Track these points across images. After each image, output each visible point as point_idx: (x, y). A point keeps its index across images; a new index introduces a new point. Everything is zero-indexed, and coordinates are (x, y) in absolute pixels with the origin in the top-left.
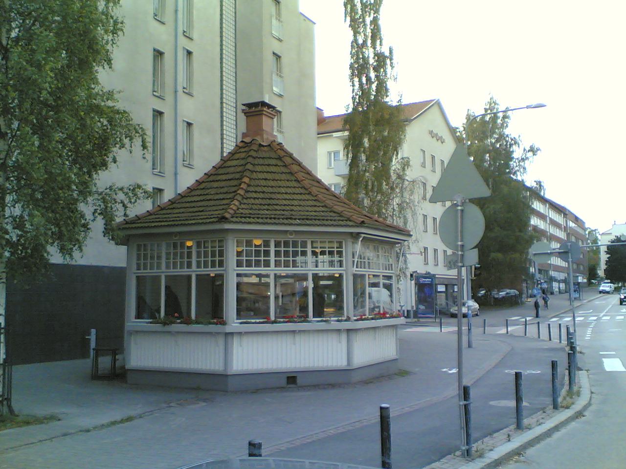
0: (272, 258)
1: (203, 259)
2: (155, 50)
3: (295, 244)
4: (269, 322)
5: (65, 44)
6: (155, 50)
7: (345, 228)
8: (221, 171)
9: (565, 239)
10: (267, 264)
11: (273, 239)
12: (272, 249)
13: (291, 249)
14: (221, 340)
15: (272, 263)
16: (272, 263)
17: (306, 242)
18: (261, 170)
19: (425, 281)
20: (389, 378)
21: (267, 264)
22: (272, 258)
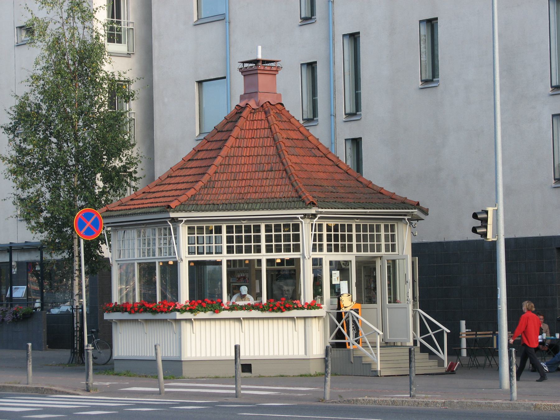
0: (263, 244)
1: (214, 245)
2: (197, 82)
3: (248, 229)
4: (71, 260)
5: (43, 178)
6: (197, 82)
7: (149, 216)
8: (169, 180)
9: (349, 163)
10: (258, 250)
11: (224, 225)
12: (263, 234)
13: (234, 235)
14: (300, 324)
15: (263, 249)
16: (263, 249)
17: (259, 226)
18: (290, 145)
19: (79, 245)
20: (341, 397)
21: (258, 250)
22: (263, 244)
